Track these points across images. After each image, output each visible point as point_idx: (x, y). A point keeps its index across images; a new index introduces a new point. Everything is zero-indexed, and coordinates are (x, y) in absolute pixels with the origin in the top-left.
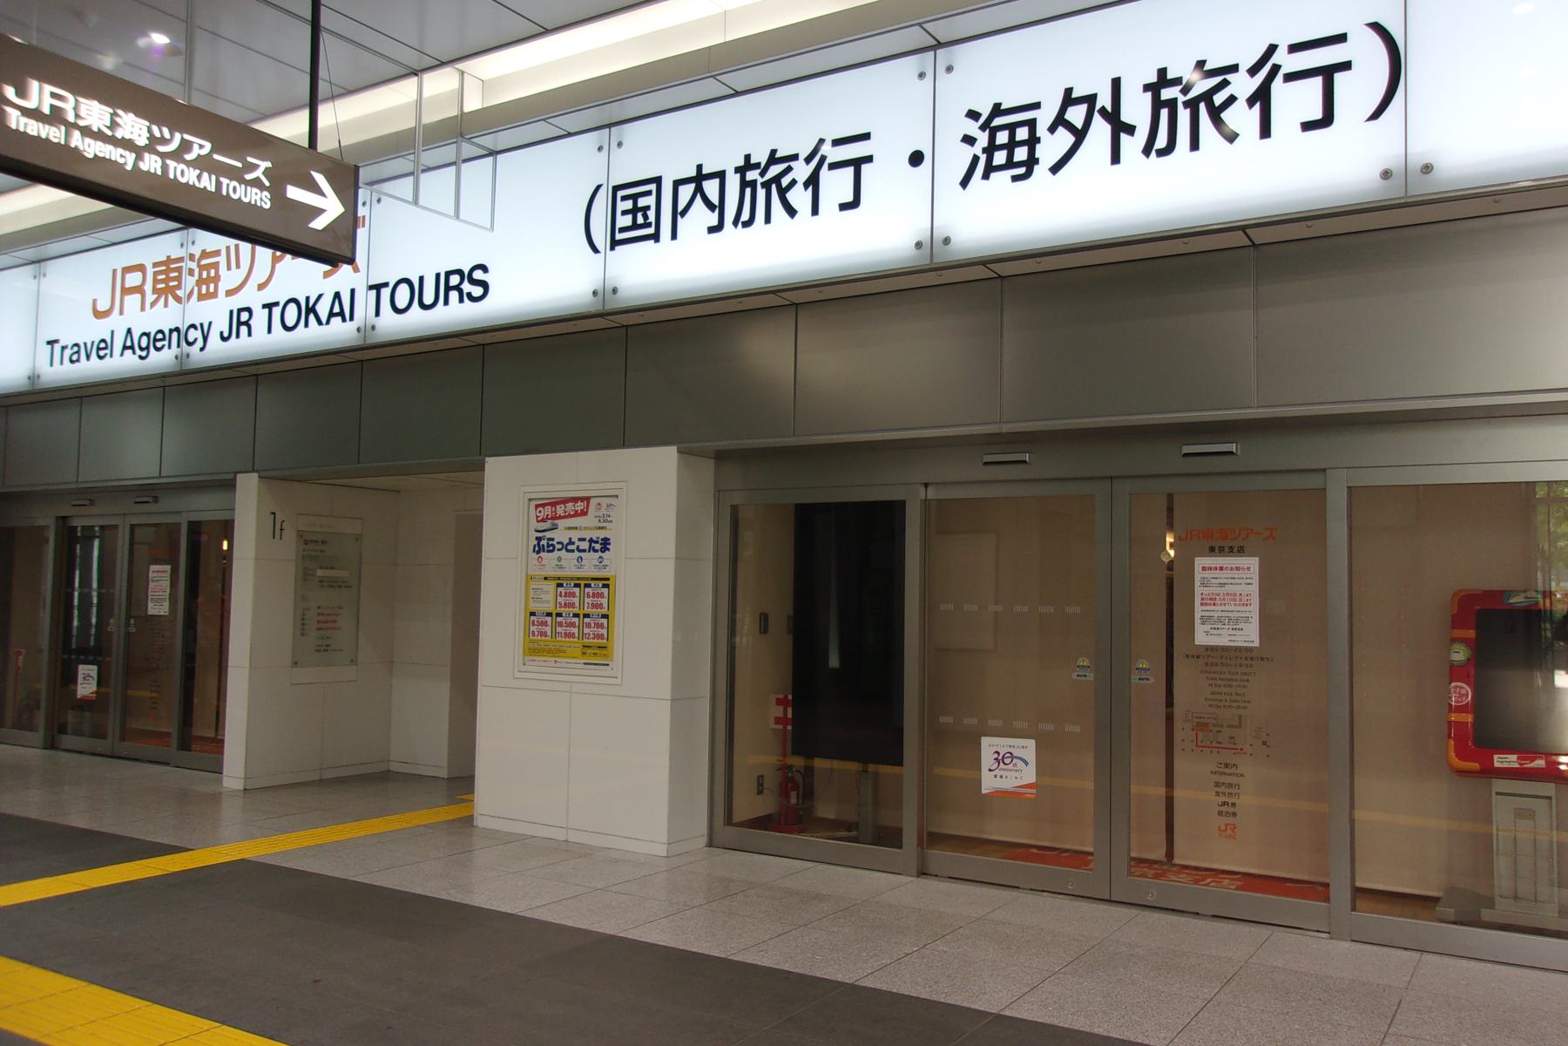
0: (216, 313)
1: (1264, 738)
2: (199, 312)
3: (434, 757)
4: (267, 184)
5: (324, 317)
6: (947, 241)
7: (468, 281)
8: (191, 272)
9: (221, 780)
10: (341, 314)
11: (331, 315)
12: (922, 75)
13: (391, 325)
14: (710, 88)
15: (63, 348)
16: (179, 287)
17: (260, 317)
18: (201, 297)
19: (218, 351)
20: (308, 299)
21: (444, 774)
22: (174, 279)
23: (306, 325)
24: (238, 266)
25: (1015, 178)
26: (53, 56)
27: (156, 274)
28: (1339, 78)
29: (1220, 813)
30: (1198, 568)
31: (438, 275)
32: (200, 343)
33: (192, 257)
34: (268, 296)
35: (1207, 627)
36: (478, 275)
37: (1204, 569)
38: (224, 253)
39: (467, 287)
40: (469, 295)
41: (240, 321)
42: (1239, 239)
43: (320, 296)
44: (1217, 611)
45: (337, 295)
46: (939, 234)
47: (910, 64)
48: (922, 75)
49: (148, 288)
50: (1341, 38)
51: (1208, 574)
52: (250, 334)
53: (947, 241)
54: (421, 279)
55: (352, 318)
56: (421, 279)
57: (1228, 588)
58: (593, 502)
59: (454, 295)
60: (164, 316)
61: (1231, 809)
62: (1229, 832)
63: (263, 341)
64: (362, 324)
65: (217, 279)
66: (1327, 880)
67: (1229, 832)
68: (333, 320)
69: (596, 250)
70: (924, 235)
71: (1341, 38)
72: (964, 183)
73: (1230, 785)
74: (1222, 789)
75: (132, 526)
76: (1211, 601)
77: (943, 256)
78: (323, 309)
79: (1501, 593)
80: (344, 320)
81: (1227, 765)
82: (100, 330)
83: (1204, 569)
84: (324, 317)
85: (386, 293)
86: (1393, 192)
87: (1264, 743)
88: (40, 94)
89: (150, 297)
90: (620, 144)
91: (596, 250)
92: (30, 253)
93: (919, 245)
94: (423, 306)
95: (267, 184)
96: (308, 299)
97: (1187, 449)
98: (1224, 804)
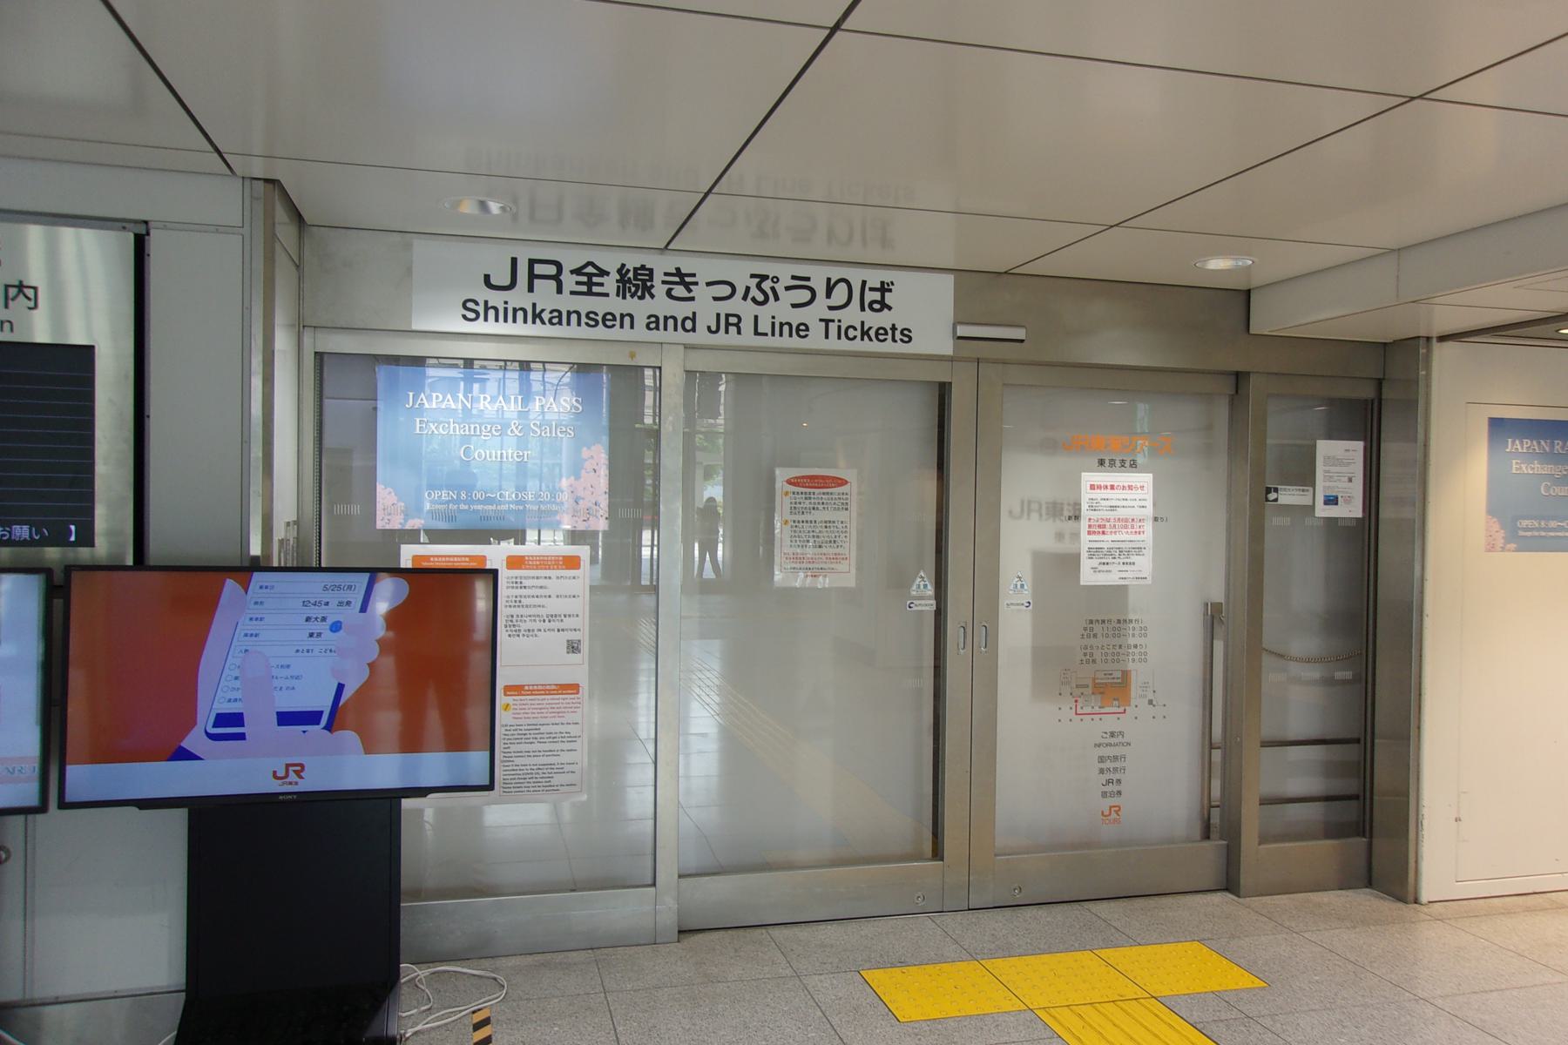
1: (1151, 696)
26: (273, 300)
29: (1104, 794)
30: (1085, 486)
35: (1095, 563)
37: (1092, 487)
44: (1106, 541)
50: (514, 261)
51: (1098, 494)
52: (739, 332)
57: (1121, 513)
61: (1115, 788)
62: (1114, 815)
67: (1114, 815)
71: (514, 261)
73: (1116, 758)
74: (1108, 764)
75: (319, 356)
79: (1517, 550)
81: (1112, 735)
83: (1092, 487)
87: (1150, 702)
98: (1109, 782)
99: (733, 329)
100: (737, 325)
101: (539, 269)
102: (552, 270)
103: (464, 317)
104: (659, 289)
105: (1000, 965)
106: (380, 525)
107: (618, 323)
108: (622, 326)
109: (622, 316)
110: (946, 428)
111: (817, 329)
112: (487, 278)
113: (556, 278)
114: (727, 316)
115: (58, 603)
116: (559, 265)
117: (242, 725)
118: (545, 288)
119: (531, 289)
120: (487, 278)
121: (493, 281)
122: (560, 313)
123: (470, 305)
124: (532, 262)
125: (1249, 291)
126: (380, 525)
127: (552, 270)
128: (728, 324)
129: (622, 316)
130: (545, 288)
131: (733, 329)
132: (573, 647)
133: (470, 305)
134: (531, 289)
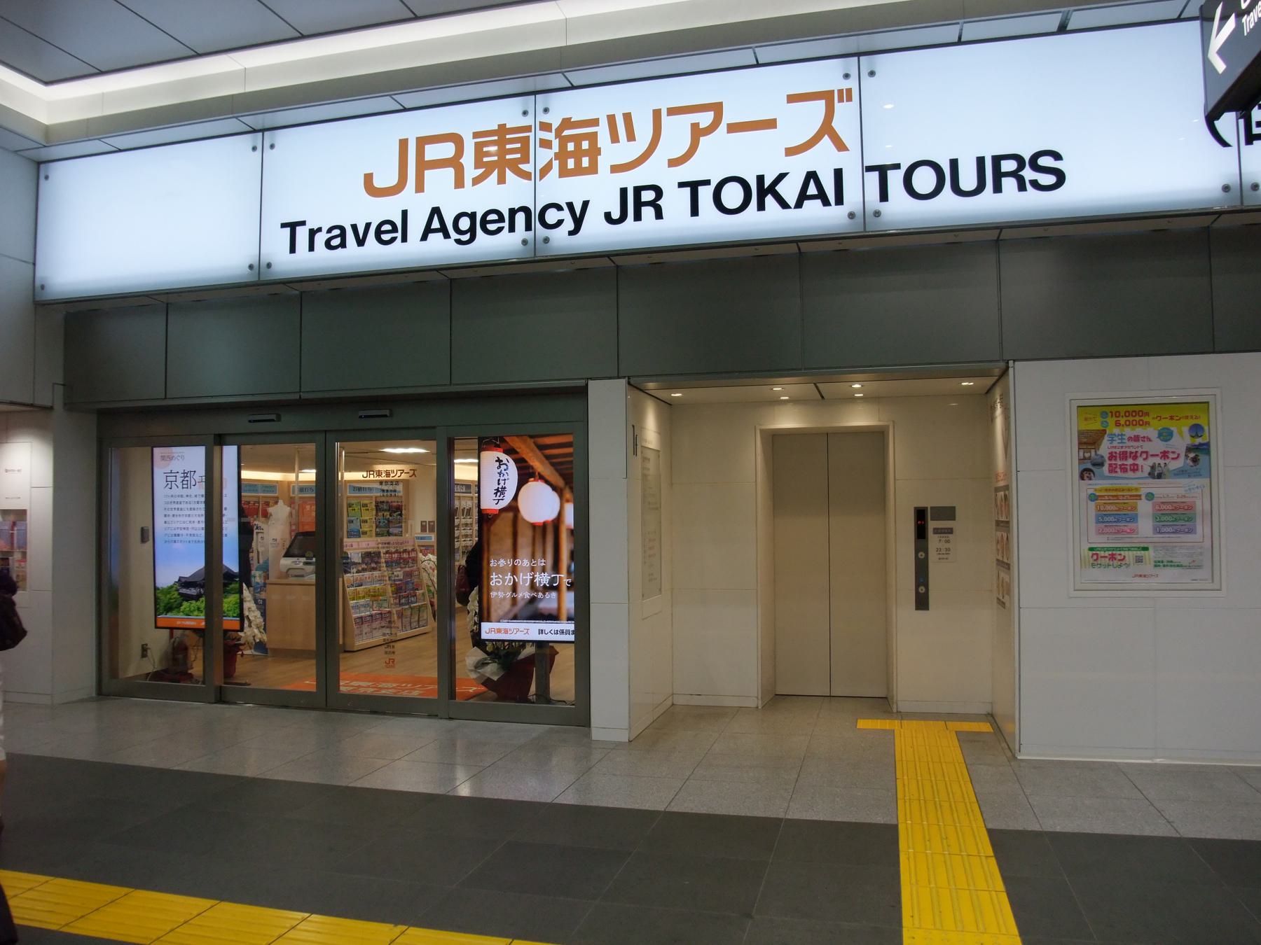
0: (601, 192)
2: (558, 189)
3: (355, 679)
5: (791, 199)
6: (269, 265)
7: (1043, 167)
8: (546, 144)
9: (588, 735)
10: (822, 196)
11: (803, 197)
12: (254, 149)
13: (901, 210)
14: (386, 103)
15: (313, 233)
16: (525, 160)
17: (676, 201)
18: (564, 173)
19: (598, 234)
20: (760, 179)
23: (761, 207)
24: (631, 137)
27: (479, 147)
28: (450, 172)
31: (981, 161)
32: (569, 224)
33: (546, 127)
34: (690, 172)
36: (1045, 161)
38: (604, 124)
39: (1028, 174)
41: (640, 201)
42: (605, 262)
43: (781, 177)
45: (812, 176)
46: (264, 261)
47: (247, 140)
48: (254, 149)
49: (468, 160)
52: (659, 215)
53: (269, 265)
54: (954, 164)
55: (839, 200)
56: (954, 164)
60: (508, 193)
63: (676, 224)
64: (857, 208)
65: (594, 152)
69: (1224, 144)
70: (255, 261)
72: (405, 213)
77: (268, 276)
78: (790, 190)
80: (826, 203)
82: (389, 209)
84: (791, 199)
85: (705, 194)
86: (528, 255)
89: (471, 172)
90: (272, 146)
91: (1224, 144)
92: (852, 44)
93: (251, 267)
94: (957, 190)
96: (760, 179)
97: (362, 413)
99: (648, 212)
101: (432, 152)
102: (448, 150)
103: (1057, 156)
106: (314, 690)
107: (506, 225)
111: (676, 201)
112: (368, 178)
113: (454, 163)
114: (997, 160)
115: (1030, 284)
117: (954, 519)
118: (438, 180)
119: (420, 188)
120: (368, 178)
121: (378, 183)
122: (342, 229)
123: (1049, 179)
125: (102, 692)
126: (314, 690)
127: (448, 150)
128: (639, 204)
129: (513, 212)
130: (438, 180)
131: (648, 212)
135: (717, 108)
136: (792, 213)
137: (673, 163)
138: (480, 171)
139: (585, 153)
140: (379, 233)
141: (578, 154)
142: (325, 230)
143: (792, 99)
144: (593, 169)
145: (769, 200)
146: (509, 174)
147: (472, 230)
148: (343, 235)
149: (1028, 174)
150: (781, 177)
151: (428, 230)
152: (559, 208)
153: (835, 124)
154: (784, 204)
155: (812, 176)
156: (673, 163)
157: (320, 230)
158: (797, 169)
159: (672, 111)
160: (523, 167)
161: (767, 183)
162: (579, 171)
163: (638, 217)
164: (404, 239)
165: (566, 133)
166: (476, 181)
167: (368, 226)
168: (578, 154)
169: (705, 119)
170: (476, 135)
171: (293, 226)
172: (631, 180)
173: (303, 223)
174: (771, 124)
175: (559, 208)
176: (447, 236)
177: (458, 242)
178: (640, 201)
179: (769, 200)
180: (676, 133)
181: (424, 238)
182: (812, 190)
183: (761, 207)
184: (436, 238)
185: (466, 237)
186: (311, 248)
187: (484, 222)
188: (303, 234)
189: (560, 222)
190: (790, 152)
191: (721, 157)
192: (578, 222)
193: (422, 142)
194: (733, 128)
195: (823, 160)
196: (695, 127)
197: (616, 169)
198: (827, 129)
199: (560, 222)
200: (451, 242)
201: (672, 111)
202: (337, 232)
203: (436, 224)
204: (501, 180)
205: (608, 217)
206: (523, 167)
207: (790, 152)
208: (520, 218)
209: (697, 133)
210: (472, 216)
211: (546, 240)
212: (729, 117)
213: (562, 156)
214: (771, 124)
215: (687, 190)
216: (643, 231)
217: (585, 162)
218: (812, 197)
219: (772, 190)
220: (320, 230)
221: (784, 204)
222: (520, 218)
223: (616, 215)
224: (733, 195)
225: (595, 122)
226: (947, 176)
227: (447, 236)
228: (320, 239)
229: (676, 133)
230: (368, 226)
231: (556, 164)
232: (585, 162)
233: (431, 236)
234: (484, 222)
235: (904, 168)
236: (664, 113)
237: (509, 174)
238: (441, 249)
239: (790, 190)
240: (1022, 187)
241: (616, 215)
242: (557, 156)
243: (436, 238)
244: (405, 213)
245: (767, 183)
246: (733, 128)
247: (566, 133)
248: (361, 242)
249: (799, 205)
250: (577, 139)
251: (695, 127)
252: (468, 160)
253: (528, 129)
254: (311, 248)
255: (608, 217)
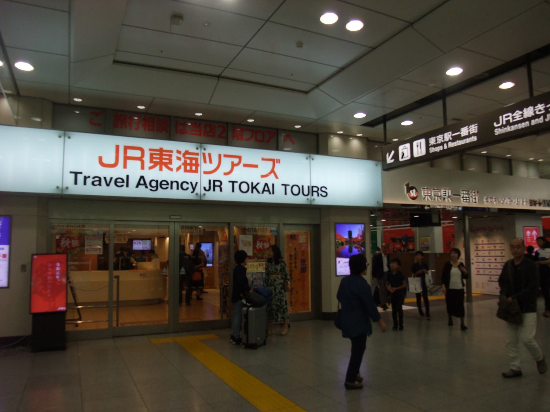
4: (393, 152)
5: (261, 191)
10: (269, 191)
11: (264, 190)
15: (86, 178)
20: (252, 183)
21: (120, 300)
22: (191, 168)
24: (211, 162)
25: (326, 188)
27: (151, 155)
28: (139, 163)
31: (309, 187)
32: (191, 189)
33: (179, 152)
34: (232, 177)
36: (323, 189)
39: (320, 192)
40: (321, 195)
43: (258, 184)
45: (266, 184)
49: (147, 159)
52: (221, 190)
53: (67, 188)
58: (54, 252)
59: (315, 194)
63: (227, 194)
65: (197, 165)
66: (405, 328)
68: (265, 192)
72: (128, 176)
76: (416, 289)
78: (260, 188)
80: (270, 193)
84: (261, 191)
85: (289, 188)
88: (503, 119)
89: (148, 164)
95: (393, 152)
96: (252, 183)
99: (217, 189)
100: (220, 186)
101: (130, 153)
102: (138, 154)
104: (176, 163)
105: (502, 63)
107: (169, 186)
108: (172, 188)
109: (172, 182)
110: (528, 177)
111: (227, 186)
112: (100, 158)
113: (141, 159)
114: (214, 181)
116: (142, 150)
119: (125, 166)
120: (100, 158)
121: (105, 161)
122: (100, 178)
123: (324, 194)
124: (126, 148)
127: (138, 154)
128: (214, 186)
129: (172, 182)
131: (217, 189)
132: (339, 262)
133: (324, 194)
134: (125, 166)
135: (240, 158)
136: (261, 195)
137: (226, 174)
138: (152, 165)
139: (194, 165)
140: (116, 182)
141: (191, 165)
142: (92, 177)
143: (263, 159)
144: (196, 171)
145: (254, 190)
146: (164, 168)
147: (157, 186)
148: (100, 181)
149: (320, 192)
150: (258, 184)
151: (139, 184)
152: (187, 183)
153: (275, 170)
154: (258, 192)
155: (266, 184)
156: (226, 174)
157: (89, 177)
158: (263, 181)
159: (226, 156)
160: (169, 166)
161: (254, 185)
162: (191, 171)
163: (214, 190)
164: (127, 186)
165: (187, 156)
166: (150, 168)
167: (111, 178)
168: (191, 165)
169: (236, 161)
170: (150, 150)
171: (76, 174)
172: (212, 177)
173: (81, 173)
174: (256, 166)
175: (187, 183)
176: (146, 187)
177: (151, 190)
178: (215, 185)
179: (254, 190)
180: (226, 164)
181: (137, 186)
182: (142, 182)
183: (252, 192)
184: (142, 187)
185: (155, 189)
186: (85, 184)
187: (161, 184)
188: (80, 178)
189: (187, 188)
190: (263, 176)
191: (241, 174)
192: (194, 189)
193: (126, 148)
194: (245, 165)
195: (270, 180)
196: (233, 163)
197: (205, 173)
198: (273, 171)
199: (187, 188)
200: (148, 190)
201: (226, 156)
202: (97, 179)
203: (266, 189)
204: (161, 169)
205: (205, 188)
206: (169, 166)
207: (263, 176)
208: (175, 185)
209: (233, 165)
210: (157, 181)
211: (204, 194)
212: (244, 161)
213: (185, 164)
214: (256, 166)
215: (73, 175)
216: (214, 196)
217: (194, 168)
218: (142, 184)
219: (255, 187)
220: (89, 177)
221: (258, 192)
222: (175, 185)
223: (207, 188)
224: (244, 187)
225: (172, 151)
226: (301, 190)
227: (146, 187)
228: (89, 181)
229: (226, 164)
230: (111, 178)
231: (183, 167)
232: (194, 168)
233: (140, 186)
234: (161, 184)
235: (239, 183)
236: (222, 156)
237: (164, 168)
238: (144, 193)
239: (260, 188)
240: (318, 195)
241: (207, 188)
242: (183, 164)
243: (142, 187)
244: (128, 176)
245: (254, 185)
246: (245, 165)
247: (187, 156)
248: (108, 185)
249: (263, 193)
250: (191, 159)
251: (233, 163)
252: (147, 159)
253: (197, 154)
254: (85, 184)
255: (205, 188)
